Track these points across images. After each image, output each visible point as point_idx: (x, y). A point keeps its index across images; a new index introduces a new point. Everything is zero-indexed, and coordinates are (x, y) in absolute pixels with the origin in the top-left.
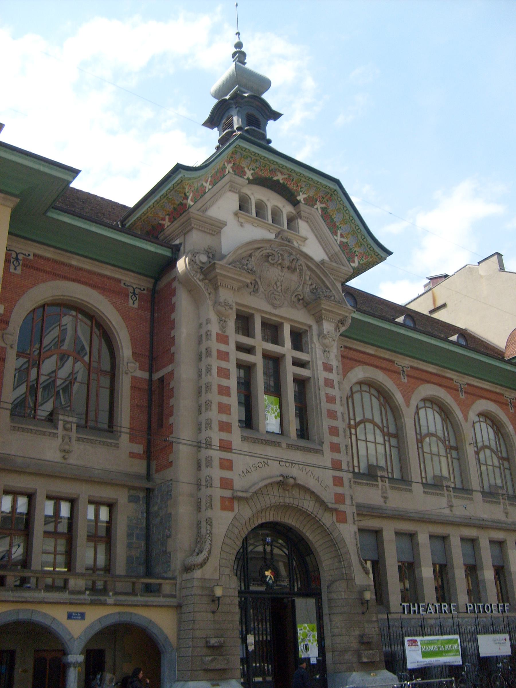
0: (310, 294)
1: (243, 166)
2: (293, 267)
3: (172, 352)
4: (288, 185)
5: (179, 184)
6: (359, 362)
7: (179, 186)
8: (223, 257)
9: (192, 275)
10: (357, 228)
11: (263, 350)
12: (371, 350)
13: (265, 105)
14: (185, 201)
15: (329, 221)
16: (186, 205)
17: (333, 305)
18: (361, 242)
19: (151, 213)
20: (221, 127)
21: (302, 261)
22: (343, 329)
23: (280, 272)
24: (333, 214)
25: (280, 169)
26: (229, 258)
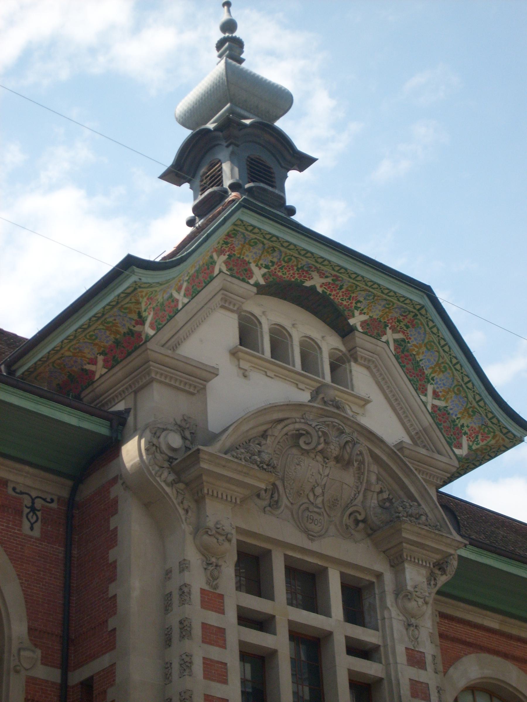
0: (380, 510)
1: (247, 259)
2: (346, 457)
3: (110, 629)
4: (332, 297)
5: (129, 294)
6: (470, 645)
7: (127, 300)
8: (213, 438)
9: (153, 472)
10: (466, 379)
11: (291, 623)
12: (492, 622)
13: (283, 142)
14: (138, 328)
15: (410, 366)
16: (139, 334)
17: (423, 532)
18: (474, 407)
19: (69, 350)
20: (197, 182)
21: (364, 445)
22: (443, 579)
23: (321, 467)
24: (418, 354)
25: (318, 266)
26: (225, 441)
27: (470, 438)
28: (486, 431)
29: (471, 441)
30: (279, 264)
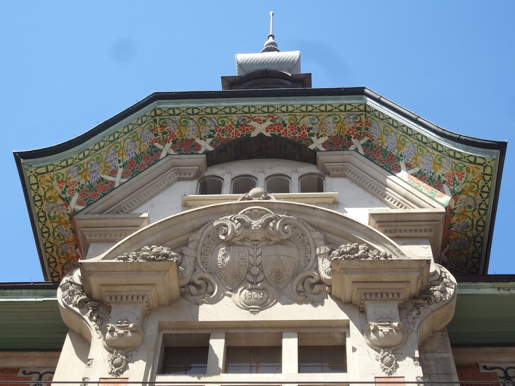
24: (383, 145)
27: (449, 184)
28: (458, 169)
29: (451, 185)
30: (218, 129)
